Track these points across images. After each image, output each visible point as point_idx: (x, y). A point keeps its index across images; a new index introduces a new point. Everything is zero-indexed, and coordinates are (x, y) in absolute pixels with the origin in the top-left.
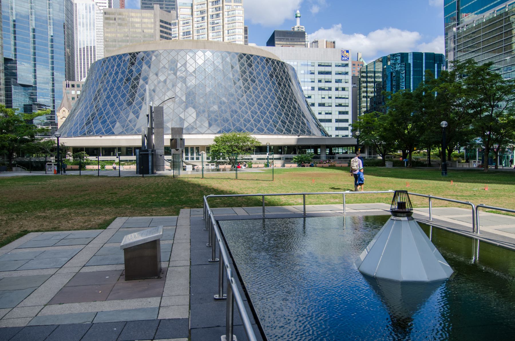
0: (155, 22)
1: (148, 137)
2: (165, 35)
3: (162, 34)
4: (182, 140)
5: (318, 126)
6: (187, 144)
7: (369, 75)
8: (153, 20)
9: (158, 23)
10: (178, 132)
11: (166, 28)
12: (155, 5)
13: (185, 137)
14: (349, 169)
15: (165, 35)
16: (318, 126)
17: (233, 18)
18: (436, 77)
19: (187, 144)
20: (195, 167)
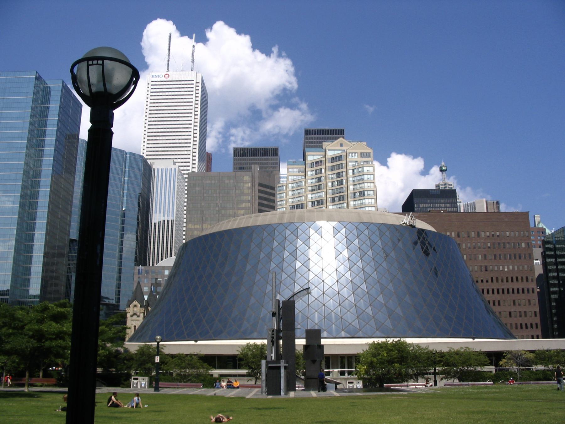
0: (253, 186)
1: (144, 362)
2: (266, 202)
3: (261, 201)
4: (321, 347)
5: (489, 311)
6: (326, 351)
7: (553, 260)
8: (250, 184)
9: (257, 187)
10: (313, 336)
11: (266, 193)
12: (253, 166)
13: (323, 342)
14: (299, 109)
15: (266, 202)
16: (489, 311)
17: (360, 177)
18: (325, 370)
19: (326, 351)
20: (338, 386)
